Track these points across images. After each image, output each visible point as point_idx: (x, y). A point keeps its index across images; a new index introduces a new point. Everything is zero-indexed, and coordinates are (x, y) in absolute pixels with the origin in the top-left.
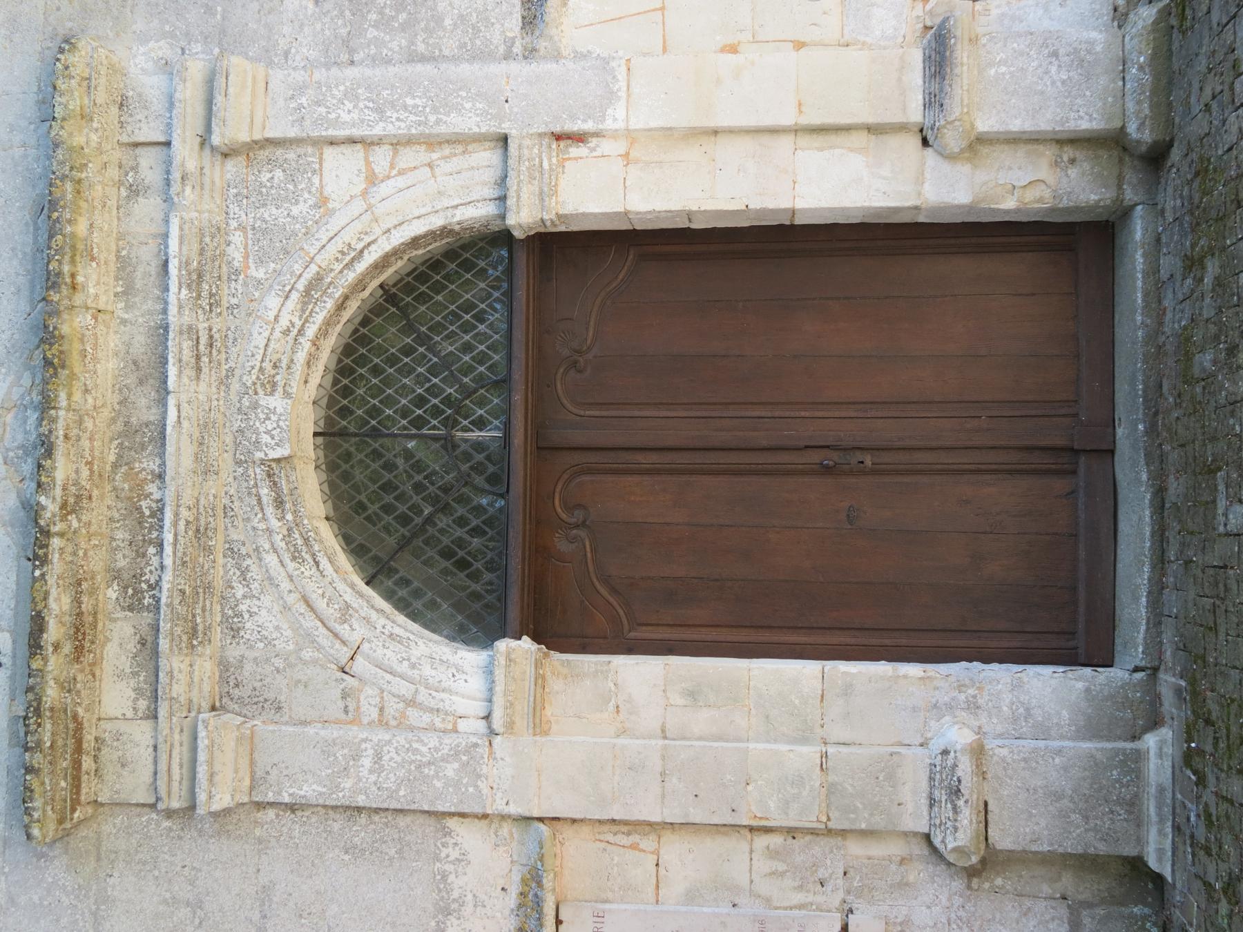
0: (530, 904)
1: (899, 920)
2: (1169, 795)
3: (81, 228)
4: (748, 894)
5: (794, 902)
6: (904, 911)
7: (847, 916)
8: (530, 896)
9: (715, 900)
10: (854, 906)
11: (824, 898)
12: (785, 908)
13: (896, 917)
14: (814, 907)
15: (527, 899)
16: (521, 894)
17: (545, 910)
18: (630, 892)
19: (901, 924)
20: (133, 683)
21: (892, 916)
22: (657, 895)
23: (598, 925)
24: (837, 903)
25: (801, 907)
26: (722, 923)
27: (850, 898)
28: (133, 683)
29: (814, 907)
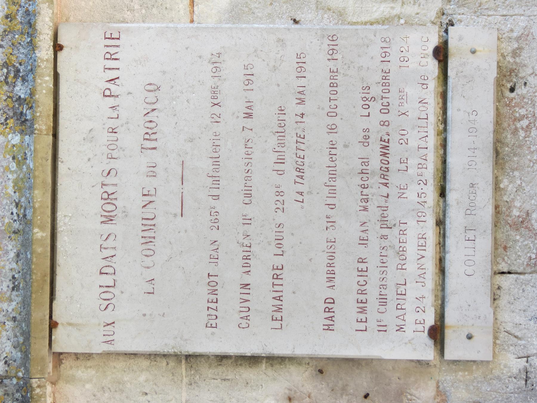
0: (19, 27)
1: (515, 35)
2: (438, 282)
3: (37, 96)
4: (313, 7)
5: (376, 15)
6: (522, 22)
7: (446, 31)
8: (19, 18)
9: (269, 16)
10: (457, 17)
11: (416, 9)
12: (362, 23)
13: (512, 31)
14: (402, 21)
15: (14, 22)
16: (7, 17)
17: (39, 26)
18: (155, 11)
19: (518, 39)
20: (230, 372)
21: (506, 30)
22: (192, 12)
23: (112, 50)
24: (432, 14)
25: (384, 21)
26: (279, 40)
27: (450, 8)
28: (230, 372)
29: (402, 21)
